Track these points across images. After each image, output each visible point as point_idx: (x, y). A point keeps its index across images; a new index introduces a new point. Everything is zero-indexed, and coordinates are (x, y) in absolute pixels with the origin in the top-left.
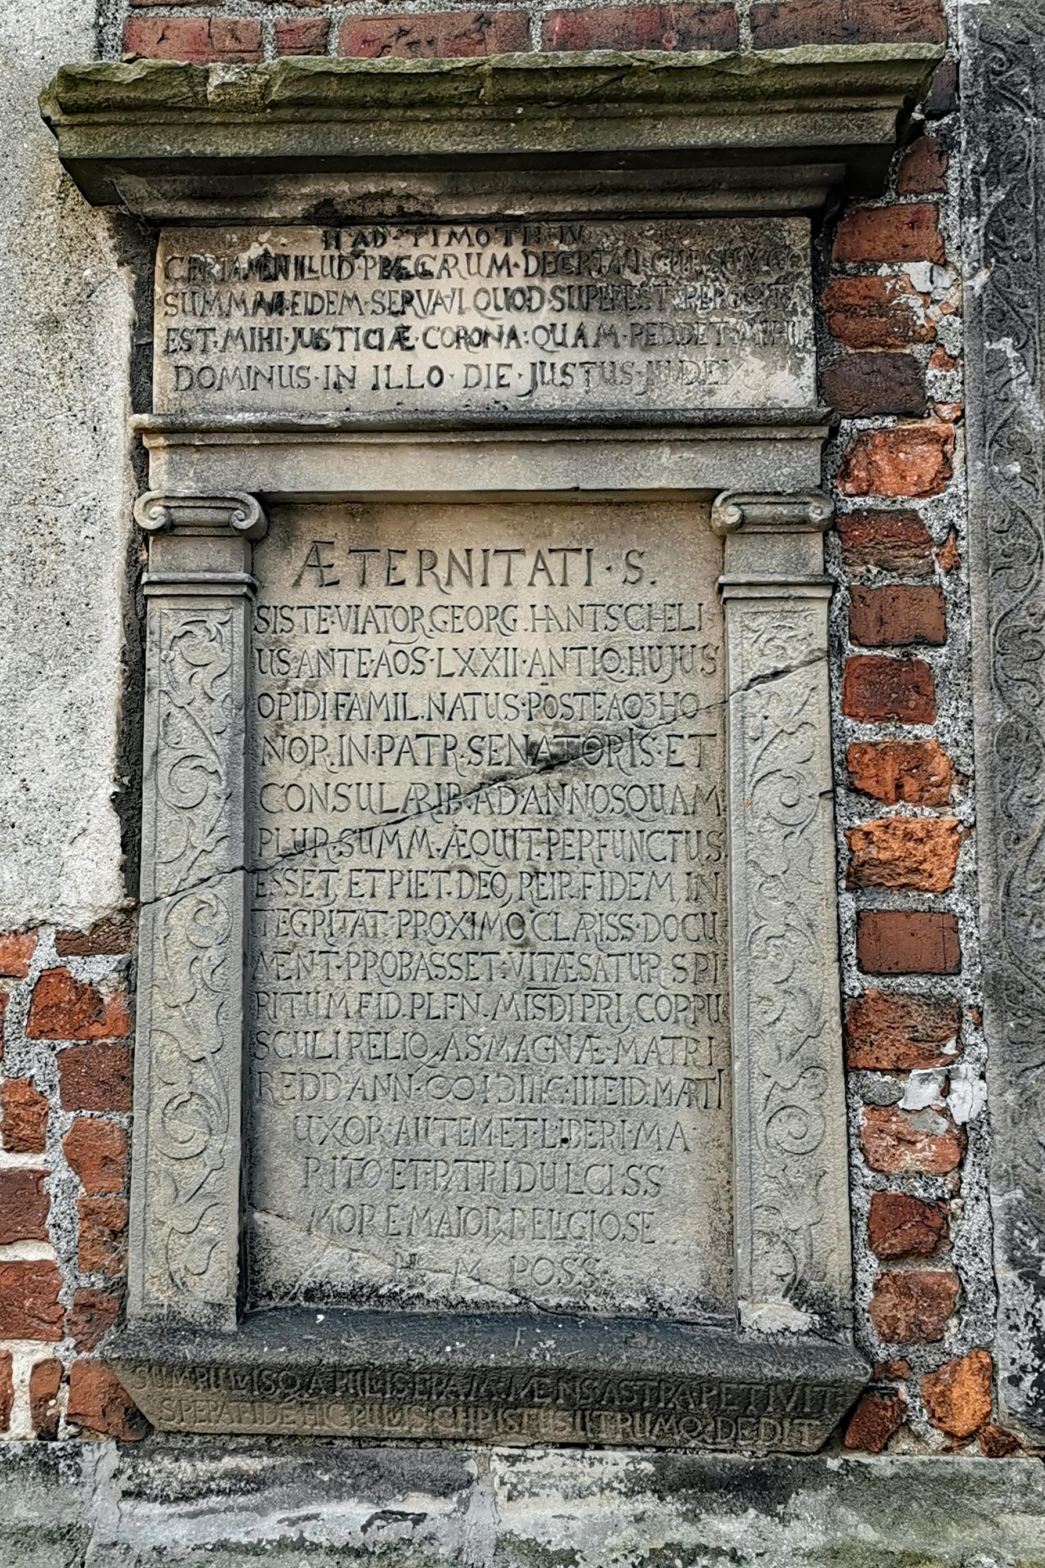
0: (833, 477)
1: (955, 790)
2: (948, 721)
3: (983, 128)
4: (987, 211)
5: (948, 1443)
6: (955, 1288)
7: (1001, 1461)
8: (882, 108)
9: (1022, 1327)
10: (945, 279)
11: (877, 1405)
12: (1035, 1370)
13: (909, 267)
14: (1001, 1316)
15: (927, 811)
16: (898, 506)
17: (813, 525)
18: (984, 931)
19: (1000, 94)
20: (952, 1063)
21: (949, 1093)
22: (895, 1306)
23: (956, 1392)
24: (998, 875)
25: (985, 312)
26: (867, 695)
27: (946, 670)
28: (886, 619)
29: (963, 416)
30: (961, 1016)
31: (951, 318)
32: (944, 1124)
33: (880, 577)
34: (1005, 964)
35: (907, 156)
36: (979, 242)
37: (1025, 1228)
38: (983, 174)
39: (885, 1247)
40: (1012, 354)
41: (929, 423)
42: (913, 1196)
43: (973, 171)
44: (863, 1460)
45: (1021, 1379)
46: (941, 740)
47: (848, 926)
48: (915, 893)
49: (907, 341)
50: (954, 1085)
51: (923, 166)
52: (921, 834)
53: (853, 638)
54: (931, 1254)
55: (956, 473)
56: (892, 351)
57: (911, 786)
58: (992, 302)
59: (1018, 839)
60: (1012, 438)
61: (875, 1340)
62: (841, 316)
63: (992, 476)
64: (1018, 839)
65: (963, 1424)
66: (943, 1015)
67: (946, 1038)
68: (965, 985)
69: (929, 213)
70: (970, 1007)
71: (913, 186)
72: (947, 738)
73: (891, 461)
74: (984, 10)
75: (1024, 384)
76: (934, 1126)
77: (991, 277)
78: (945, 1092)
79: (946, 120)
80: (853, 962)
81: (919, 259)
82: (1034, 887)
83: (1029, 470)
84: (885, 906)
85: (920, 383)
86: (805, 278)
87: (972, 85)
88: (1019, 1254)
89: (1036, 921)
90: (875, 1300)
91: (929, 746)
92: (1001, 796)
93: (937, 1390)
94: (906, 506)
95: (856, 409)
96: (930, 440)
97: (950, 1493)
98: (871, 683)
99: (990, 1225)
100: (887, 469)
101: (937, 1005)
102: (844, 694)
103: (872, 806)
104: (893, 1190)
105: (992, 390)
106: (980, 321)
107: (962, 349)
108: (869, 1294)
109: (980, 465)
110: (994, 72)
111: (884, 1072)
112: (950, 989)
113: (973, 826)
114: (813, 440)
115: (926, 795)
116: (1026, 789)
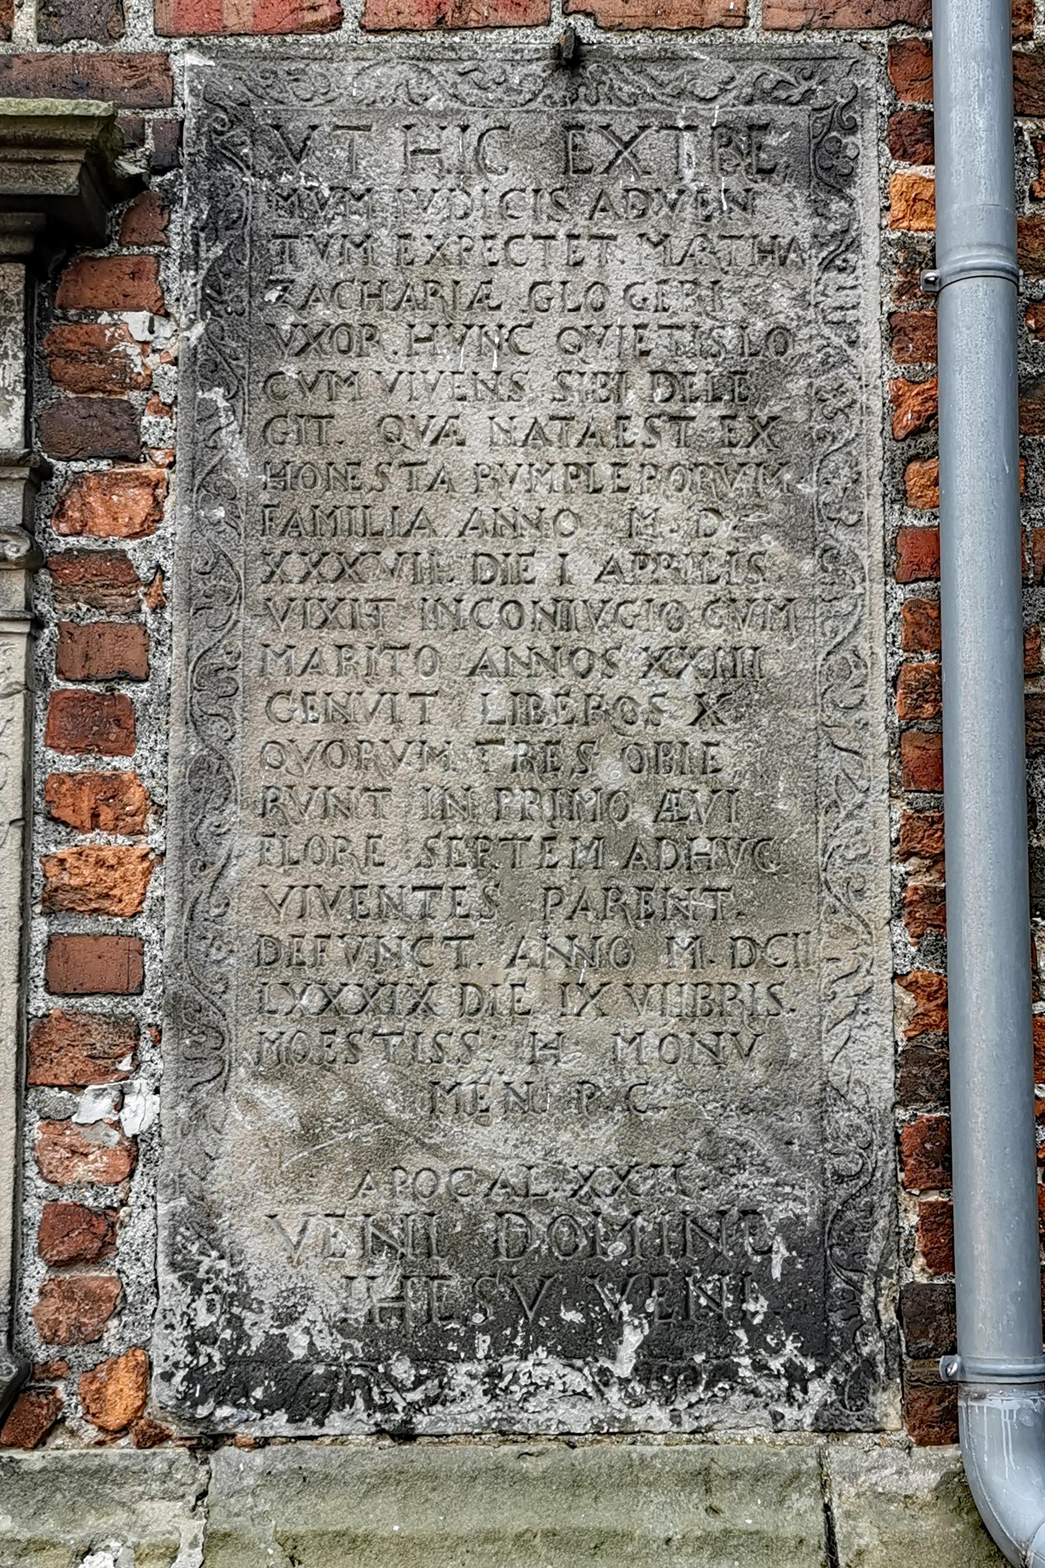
0: (47, 517)
1: (150, 818)
2: (146, 754)
3: (204, 185)
4: (206, 265)
5: (101, 1436)
6: (116, 1291)
7: (147, 1452)
8: (64, 161)
9: (177, 1326)
10: (164, 329)
11: (32, 1404)
12: (187, 1366)
13: (128, 317)
14: (158, 1316)
15: (121, 839)
16: (109, 547)
17: (11, 562)
18: (167, 953)
19: (221, 153)
20: (127, 1078)
21: (122, 1107)
22: (58, 1309)
23: (111, 1389)
24: (184, 901)
25: (199, 363)
26: (69, 727)
27: (146, 704)
28: (90, 653)
29: (174, 462)
30: (138, 1034)
31: (167, 367)
32: (116, 1136)
33: (90, 614)
34: (186, 985)
35: (131, 209)
36: (196, 295)
37: (188, 1234)
38: (203, 229)
39: (53, 1255)
40: (222, 404)
41: (145, 468)
42: (82, 1206)
43: (193, 227)
44: (17, 1457)
45: (173, 1375)
46: (138, 771)
47: (39, 949)
48: (106, 917)
49: (125, 387)
50: (128, 1099)
51: (147, 220)
52: (112, 861)
53: (59, 672)
54: (97, 1259)
55: (167, 516)
56: (113, 397)
57: (106, 815)
58: (206, 353)
59: (204, 866)
60: (218, 484)
61: (36, 1342)
62: (61, 361)
63: (198, 520)
64: (204, 866)
65: (115, 1418)
66: (121, 1034)
67: (123, 1055)
68: (146, 1005)
69: (150, 264)
70: (150, 1025)
71: (135, 237)
72: (144, 770)
73: (104, 503)
74: (208, 71)
75: (233, 433)
76: (106, 1139)
77: (206, 329)
78: (119, 1106)
79: (169, 175)
80: (40, 983)
81: (138, 308)
82: (217, 911)
83: (233, 515)
84: (76, 930)
85: (135, 429)
86: (17, 323)
87: (195, 143)
88: (180, 1258)
89: (217, 944)
90: (40, 1304)
91: (125, 778)
92: (191, 825)
93: (93, 1387)
94: (117, 546)
95: (72, 451)
96: (142, 484)
97: (93, 1483)
98: (73, 716)
99: (154, 1231)
100: (100, 510)
101: (116, 1024)
102: (47, 726)
103: (68, 834)
104: (65, 1199)
105: (201, 438)
106: (194, 371)
107: (176, 397)
108: (34, 1298)
109: (187, 509)
110: (215, 131)
111: (61, 1088)
112: (131, 1008)
113: (163, 854)
114: (15, 480)
115: (121, 824)
116: (214, 819)
